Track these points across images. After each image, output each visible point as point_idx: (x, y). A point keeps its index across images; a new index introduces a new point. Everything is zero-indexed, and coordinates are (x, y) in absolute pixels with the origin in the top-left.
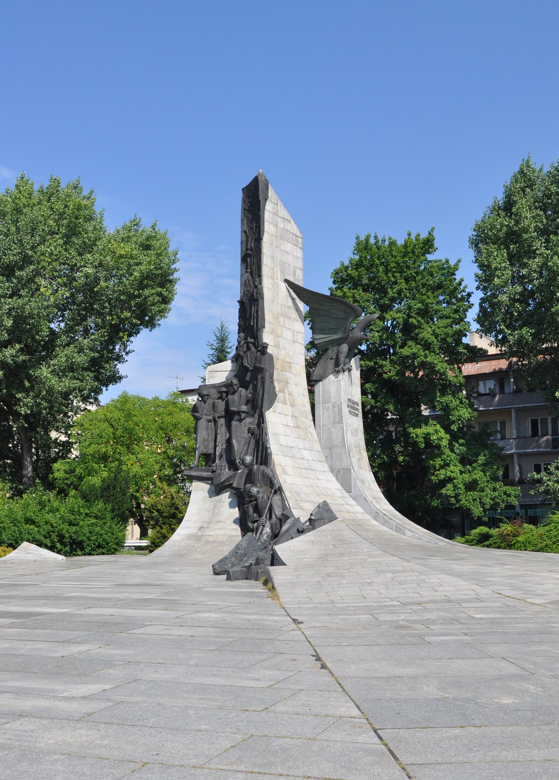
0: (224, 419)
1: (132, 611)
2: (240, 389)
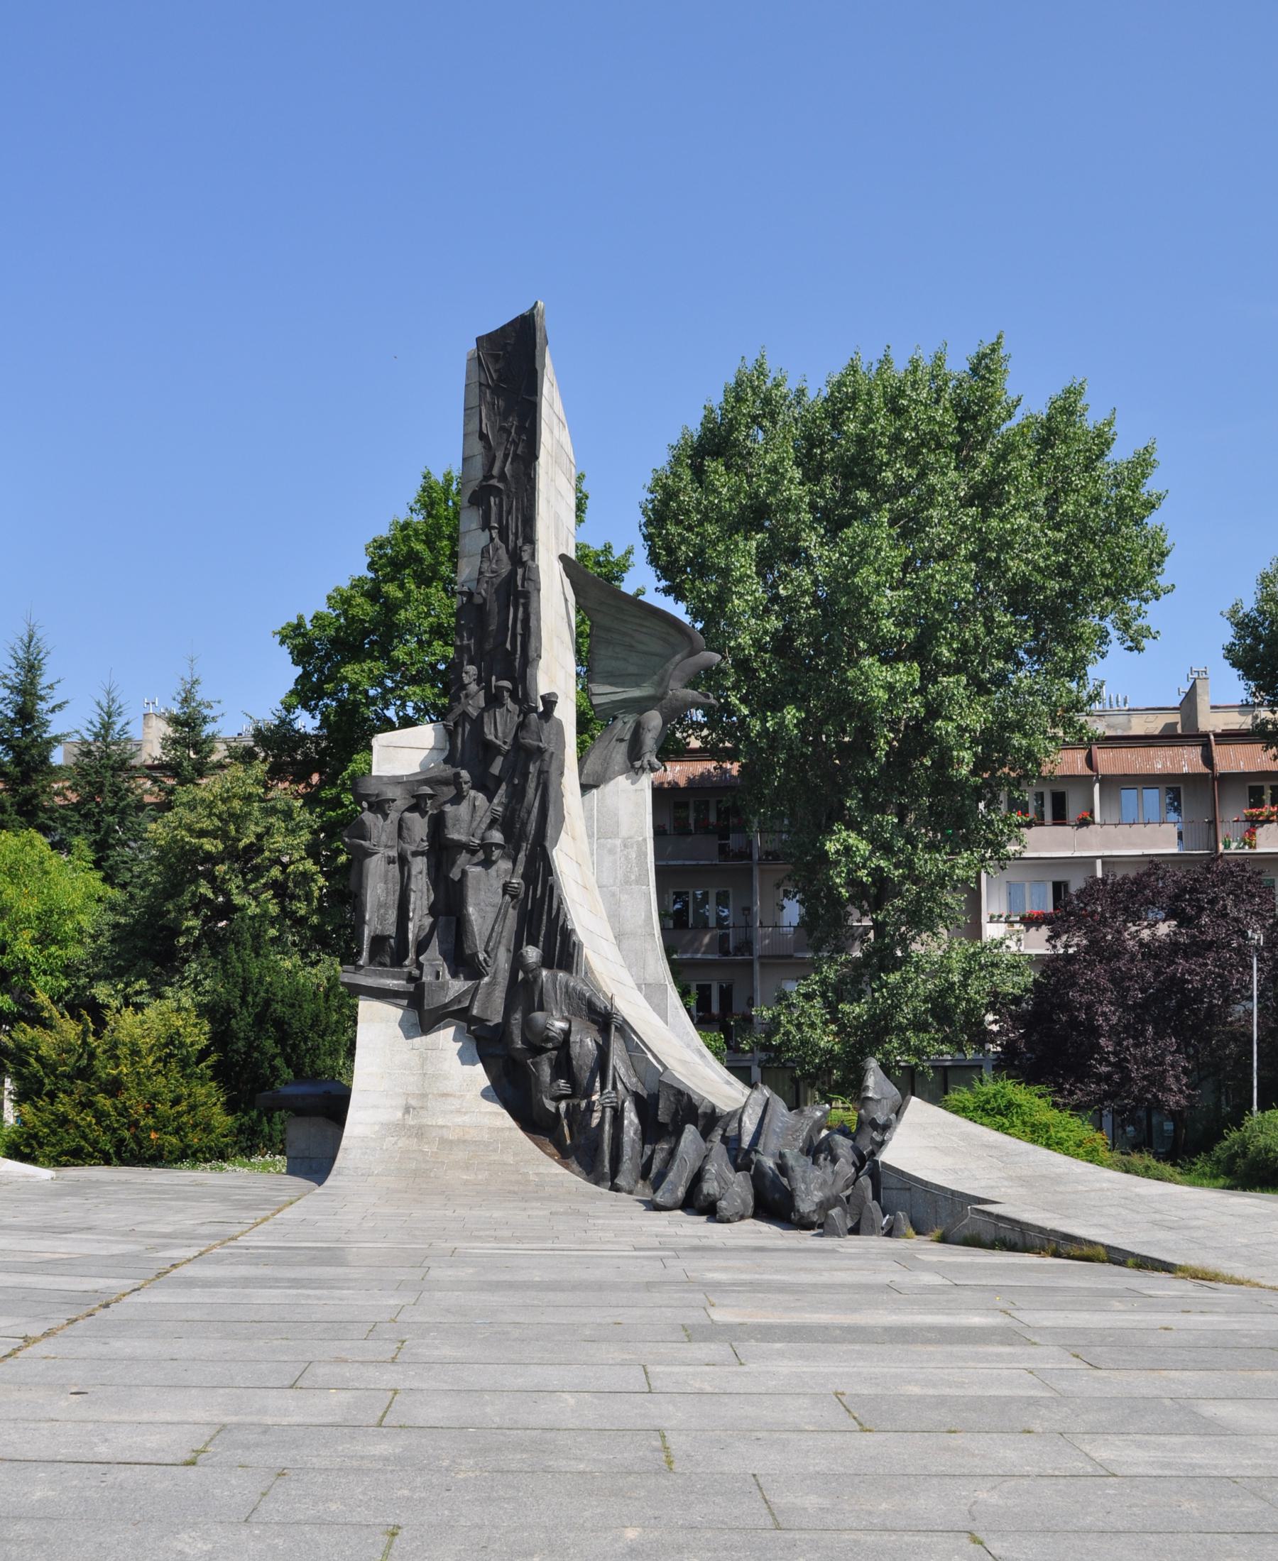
0: (425, 859)
1: (823, 1316)
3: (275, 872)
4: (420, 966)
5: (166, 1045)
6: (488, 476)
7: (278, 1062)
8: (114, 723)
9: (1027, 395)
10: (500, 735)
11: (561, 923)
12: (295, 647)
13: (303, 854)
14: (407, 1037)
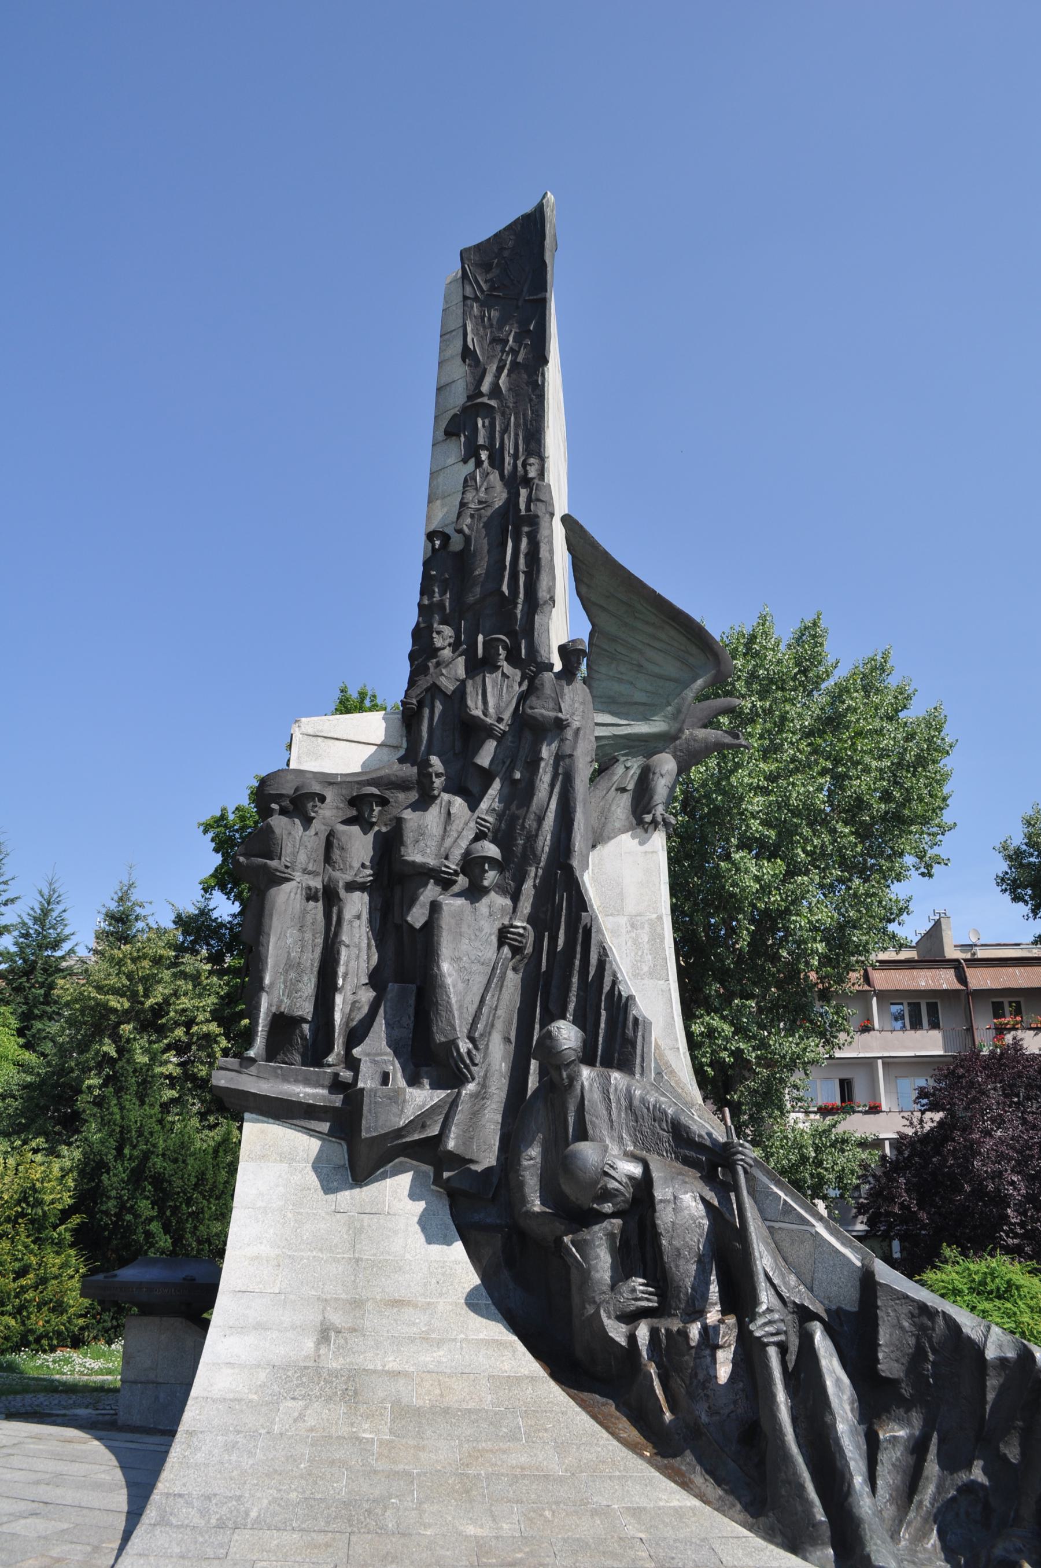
0: (366, 897)
2: (443, 794)
3: (179, 1032)
4: (353, 1064)
5: (18, 1203)
7: (155, 1227)
8: (52, 910)
9: (842, 658)
10: (491, 710)
11: (606, 988)
12: (217, 835)
13: (208, 1015)
14: (328, 1190)
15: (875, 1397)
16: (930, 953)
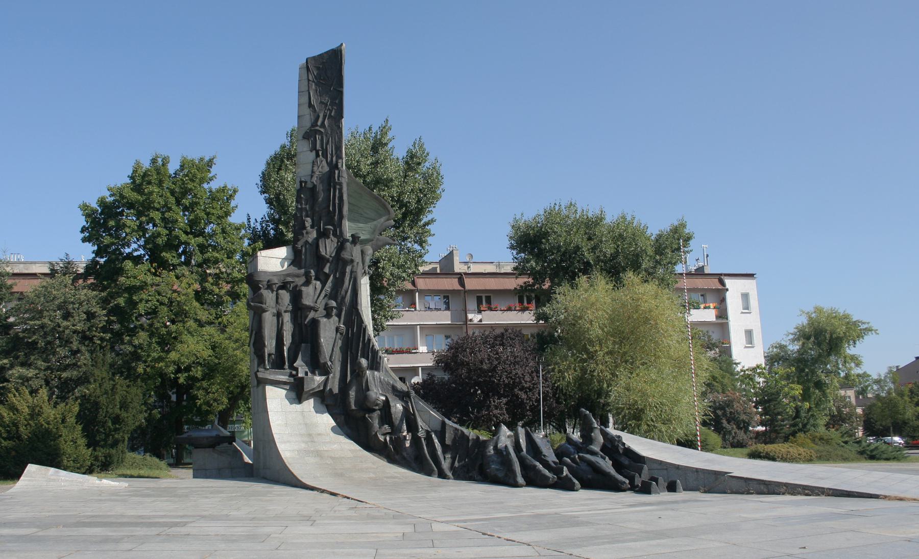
6: (314, 124)
15: (445, 448)
16: (446, 267)
